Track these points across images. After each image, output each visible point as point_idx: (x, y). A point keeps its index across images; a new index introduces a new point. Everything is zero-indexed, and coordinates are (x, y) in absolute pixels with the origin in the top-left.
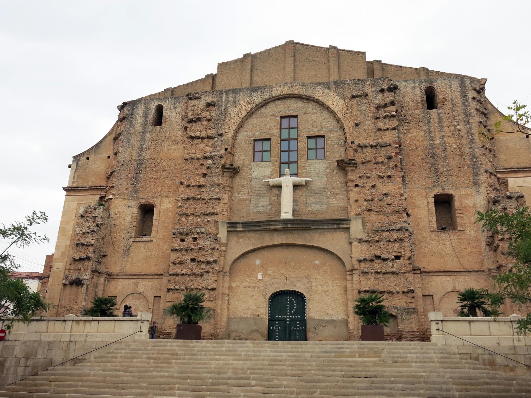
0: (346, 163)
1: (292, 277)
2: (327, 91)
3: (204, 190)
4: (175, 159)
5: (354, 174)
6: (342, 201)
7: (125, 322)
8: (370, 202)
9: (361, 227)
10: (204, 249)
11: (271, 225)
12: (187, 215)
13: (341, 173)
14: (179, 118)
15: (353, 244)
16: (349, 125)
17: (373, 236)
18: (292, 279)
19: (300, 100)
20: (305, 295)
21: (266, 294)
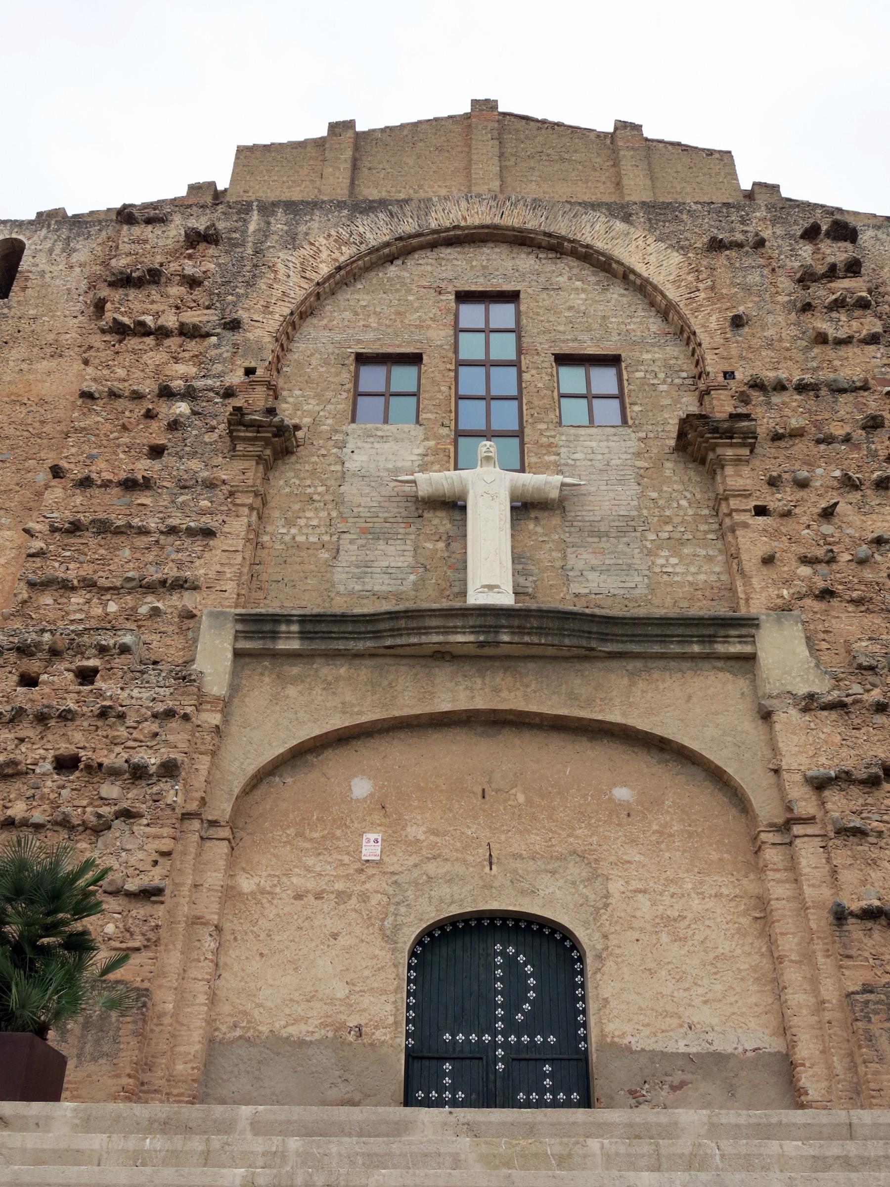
0: (715, 430)
1: (518, 856)
2: (619, 226)
3: (147, 501)
4: (43, 402)
5: (746, 471)
6: (705, 568)
8: (822, 568)
9: (803, 651)
10: (122, 716)
11: (427, 630)
12: (66, 586)
13: (692, 473)
14: (79, 281)
15: (780, 718)
16: (708, 324)
17: (857, 688)
18: (518, 865)
19: (526, 249)
20: (580, 934)
21: (396, 928)
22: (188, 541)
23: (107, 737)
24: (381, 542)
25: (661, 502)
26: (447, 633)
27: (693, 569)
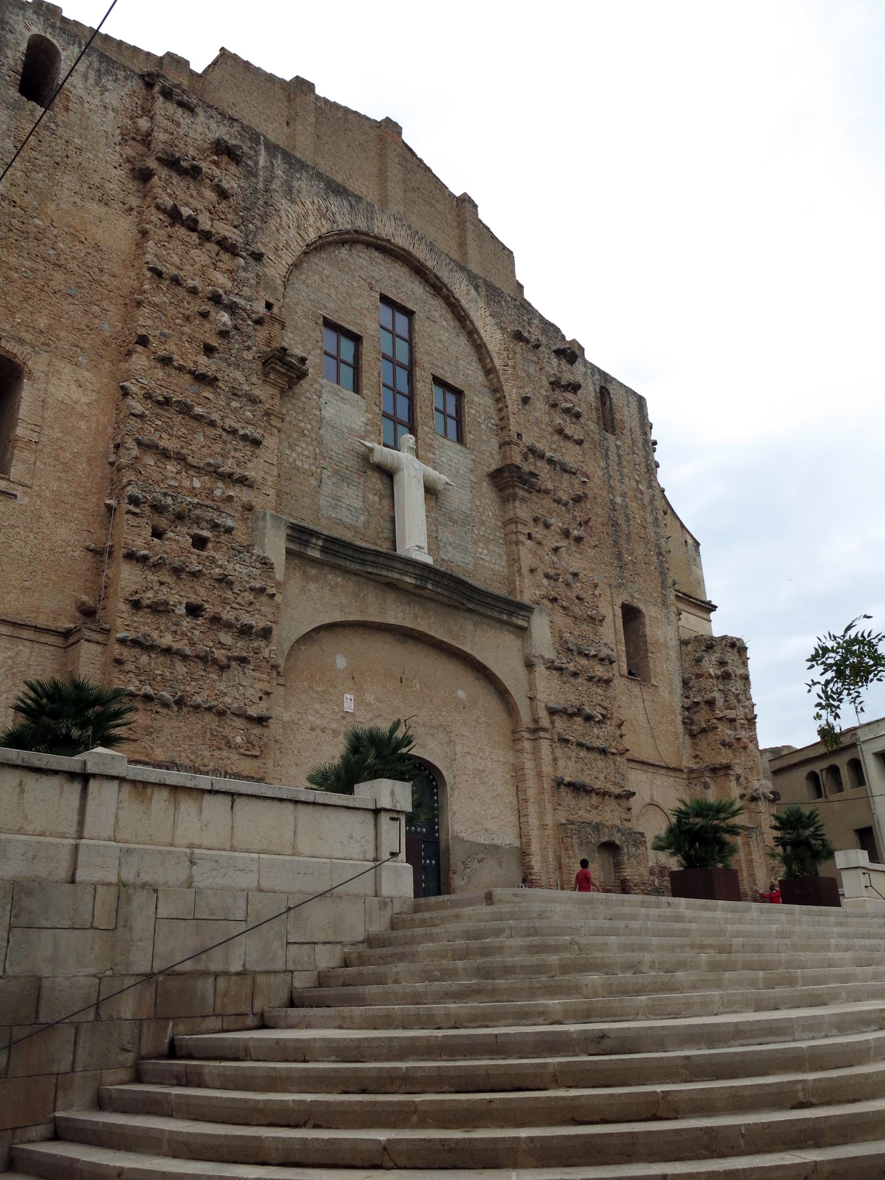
0: (519, 478)
2: (473, 292)
3: (211, 396)
4: (98, 248)
7: (330, 813)
12: (165, 454)
16: (512, 393)
20: (445, 773)
22: (241, 445)
23: (220, 596)
24: (345, 484)
25: (481, 509)
26: (402, 574)
27: (493, 561)
